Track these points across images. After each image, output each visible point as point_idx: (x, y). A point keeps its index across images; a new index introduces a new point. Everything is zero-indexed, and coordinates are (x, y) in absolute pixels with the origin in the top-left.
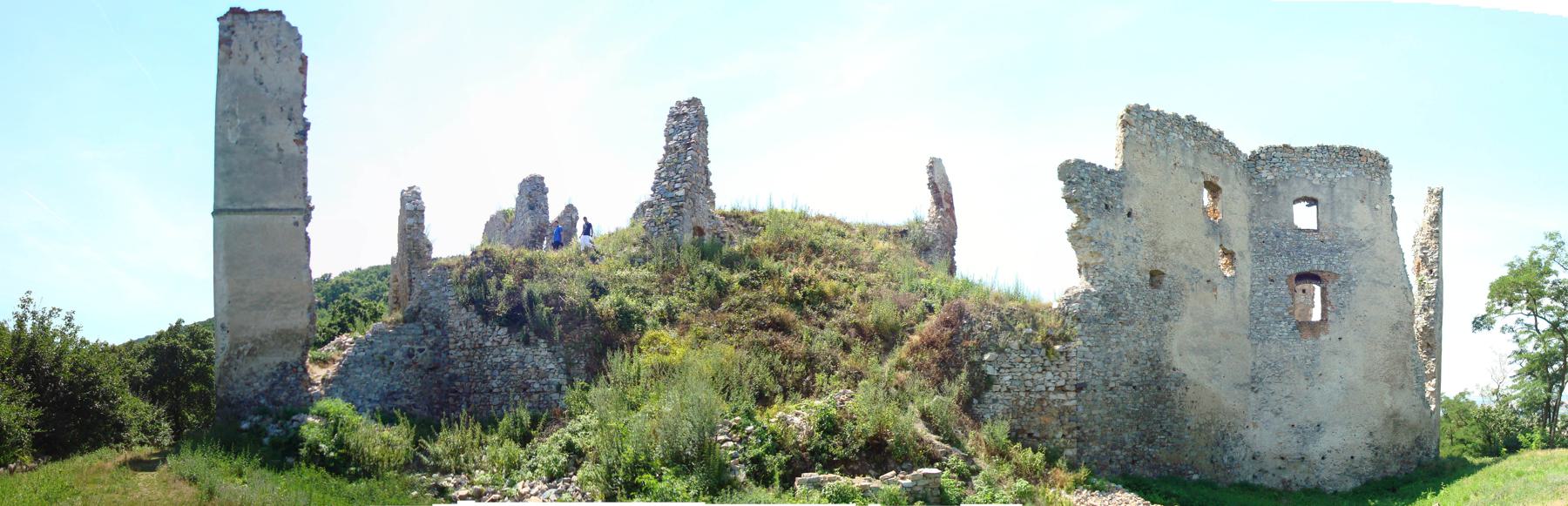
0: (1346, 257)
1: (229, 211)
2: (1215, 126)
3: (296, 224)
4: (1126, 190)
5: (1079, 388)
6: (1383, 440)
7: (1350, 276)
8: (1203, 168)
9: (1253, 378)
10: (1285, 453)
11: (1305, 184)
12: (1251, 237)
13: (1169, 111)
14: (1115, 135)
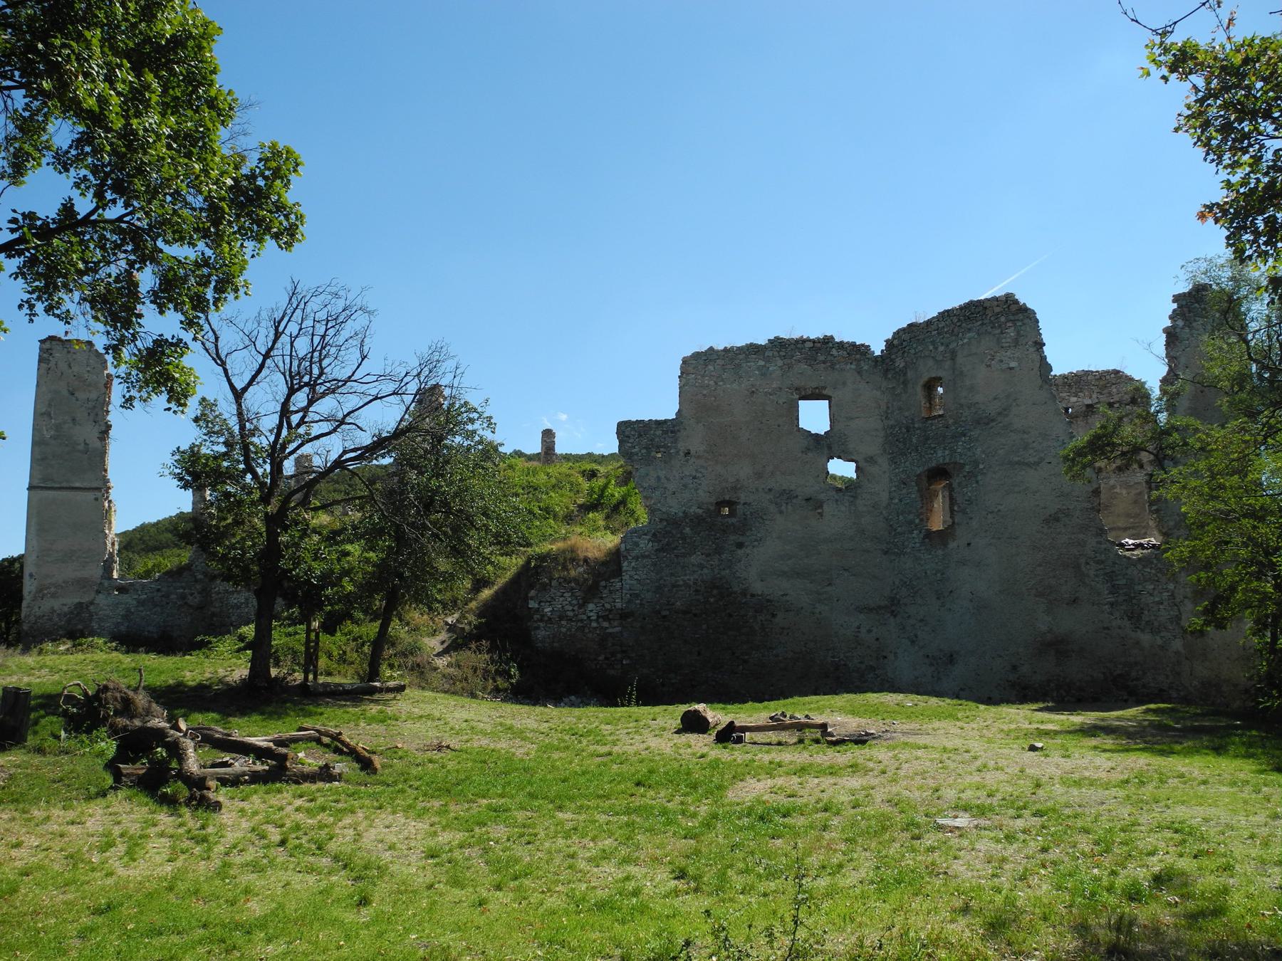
1: (42, 488)
3: (96, 499)
13: (740, 342)
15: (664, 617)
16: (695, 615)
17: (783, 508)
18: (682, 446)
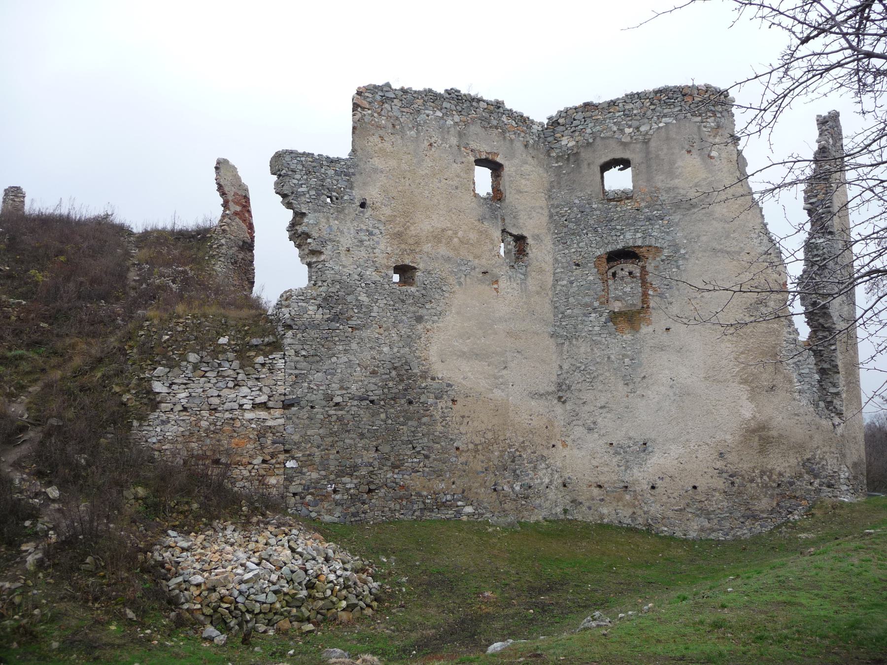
0: (670, 225)
2: (489, 95)
4: (357, 180)
5: (287, 406)
6: (745, 462)
7: (676, 248)
8: (473, 145)
9: (559, 385)
10: (602, 479)
11: (612, 143)
12: (551, 216)
13: (418, 87)
14: (343, 120)
15: (337, 404)
16: (372, 402)
17: (462, 280)
18: (357, 194)
